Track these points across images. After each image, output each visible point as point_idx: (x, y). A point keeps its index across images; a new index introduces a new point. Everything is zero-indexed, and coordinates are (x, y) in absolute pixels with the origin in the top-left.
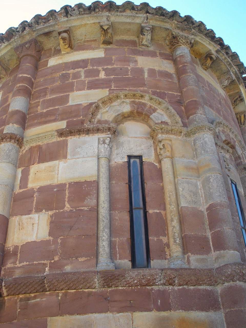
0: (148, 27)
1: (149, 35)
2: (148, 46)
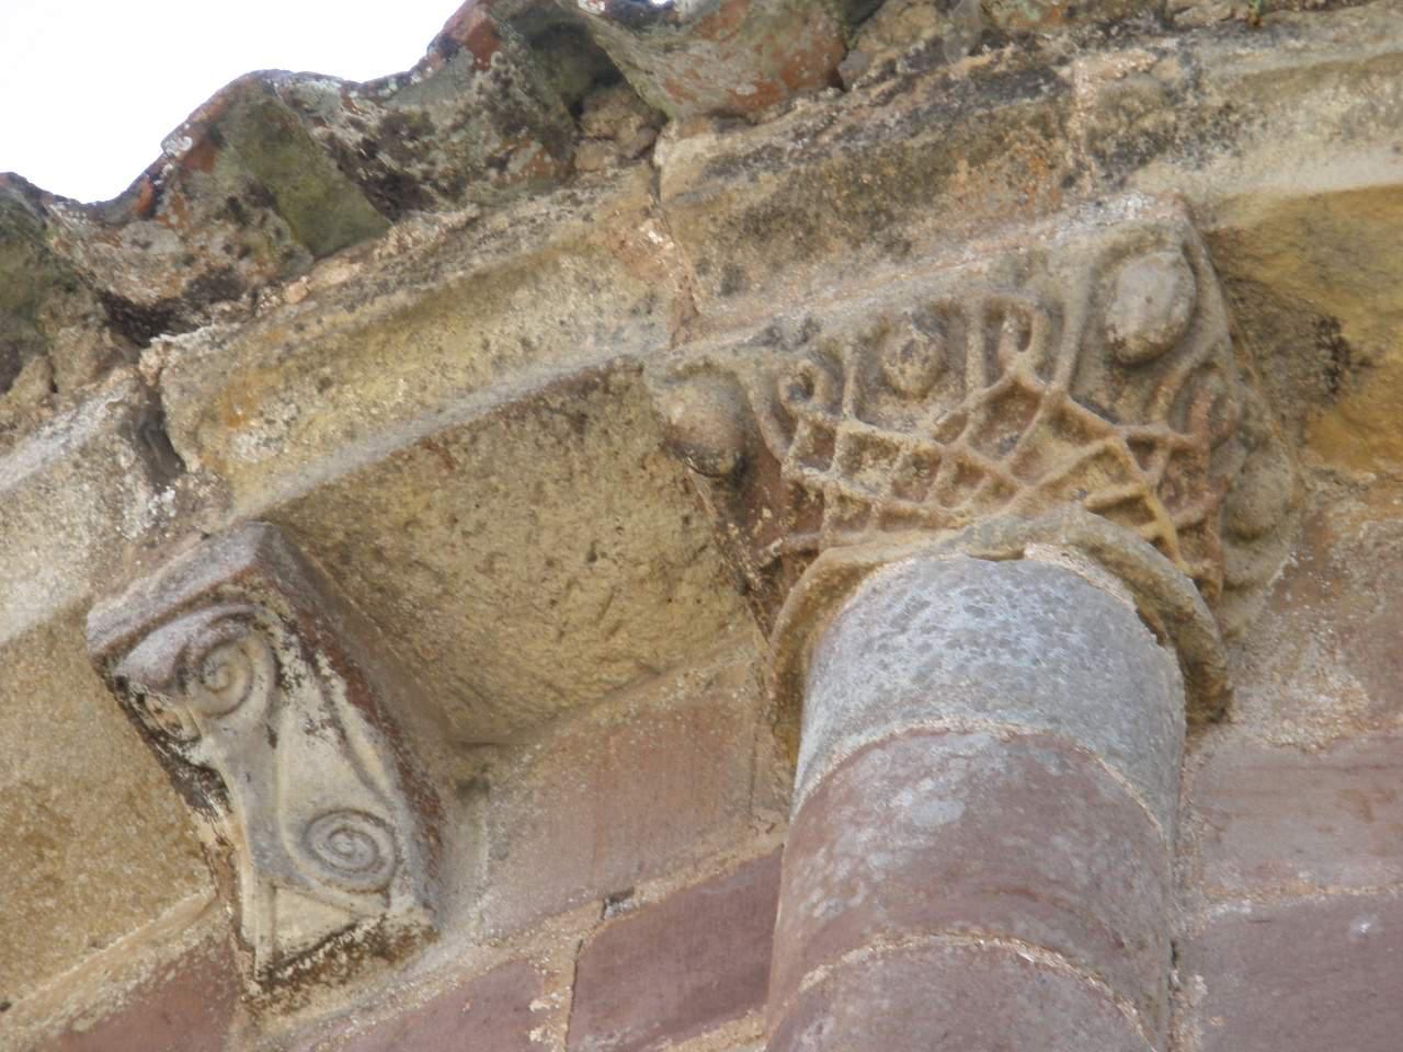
0: (190, 605)
1: (289, 723)
2: (386, 949)
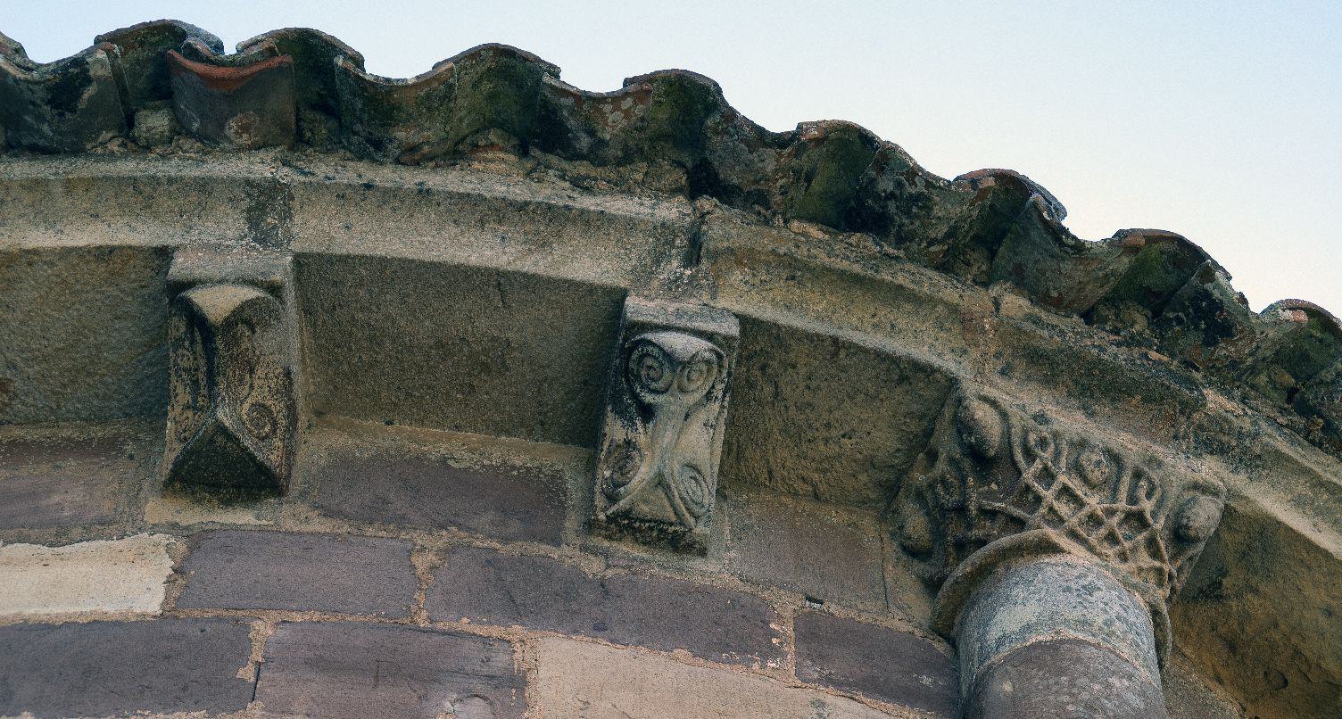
1: (702, 416)
